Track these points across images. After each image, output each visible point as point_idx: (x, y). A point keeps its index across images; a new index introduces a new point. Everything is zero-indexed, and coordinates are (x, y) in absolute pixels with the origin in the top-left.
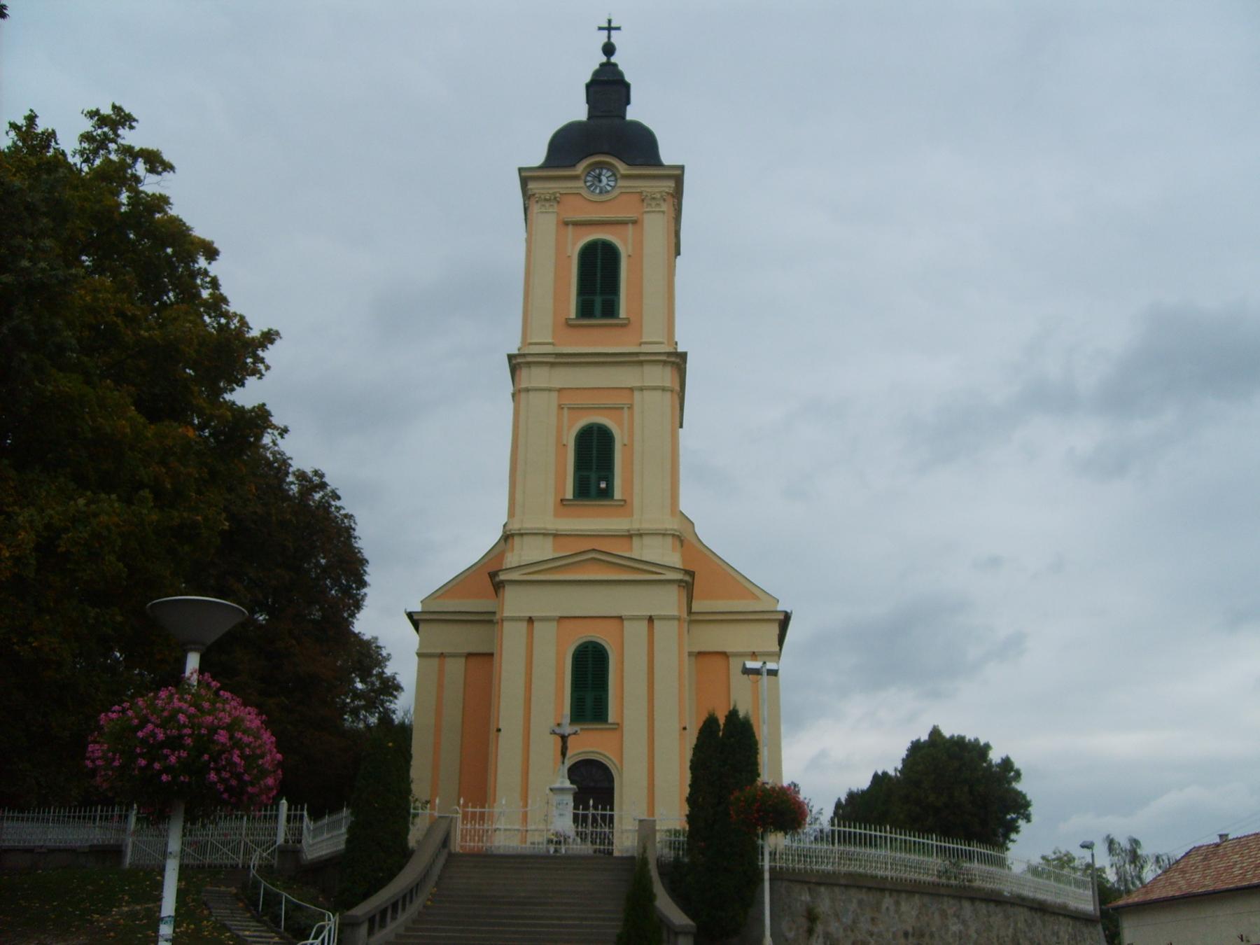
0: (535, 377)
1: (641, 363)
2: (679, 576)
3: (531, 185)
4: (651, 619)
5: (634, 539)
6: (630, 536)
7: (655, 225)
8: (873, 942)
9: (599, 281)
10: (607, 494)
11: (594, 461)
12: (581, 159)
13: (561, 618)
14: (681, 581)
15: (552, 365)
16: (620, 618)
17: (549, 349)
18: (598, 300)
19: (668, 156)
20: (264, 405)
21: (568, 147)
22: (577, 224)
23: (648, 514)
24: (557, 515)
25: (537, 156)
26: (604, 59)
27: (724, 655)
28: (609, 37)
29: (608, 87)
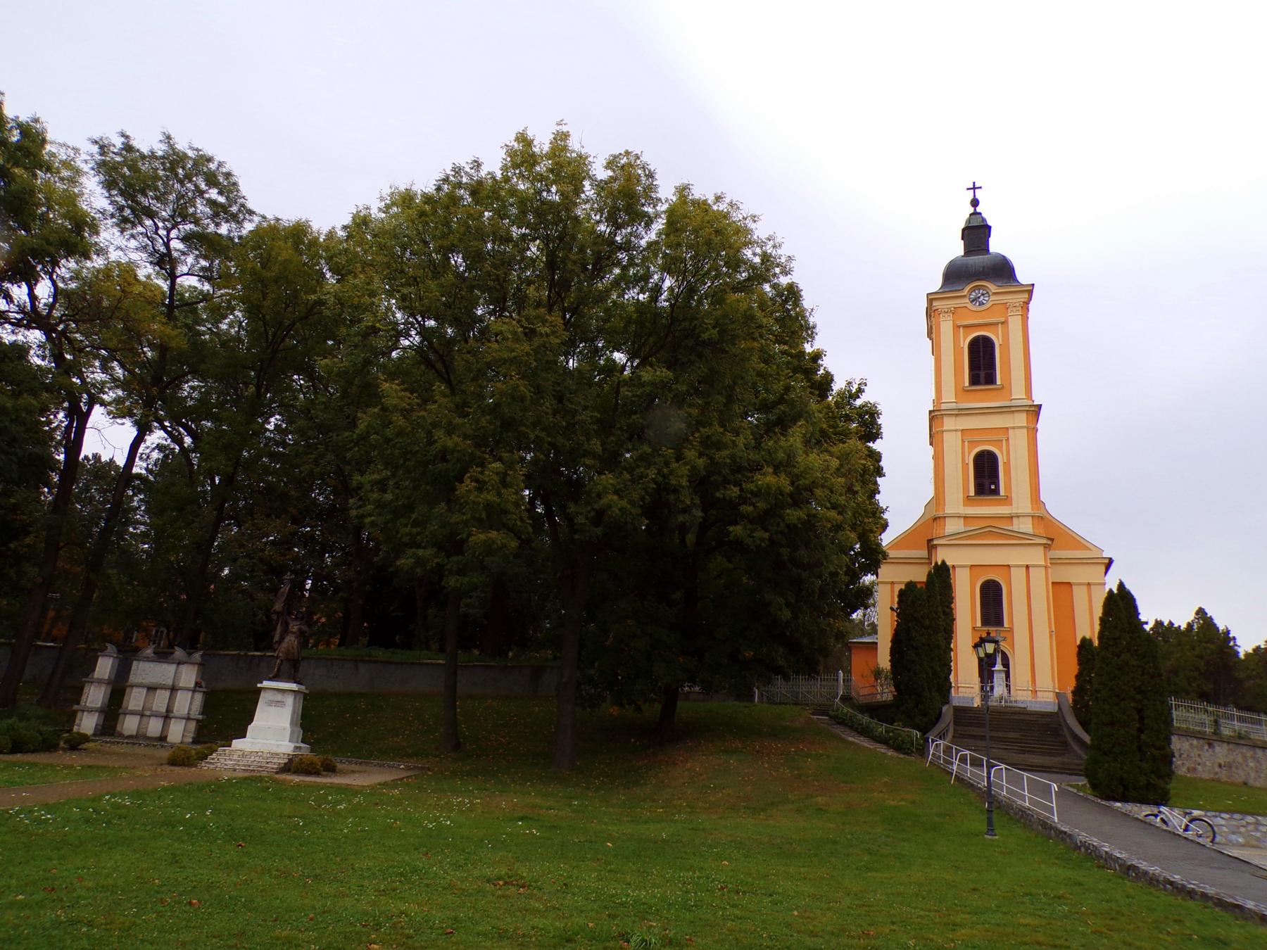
2: (1045, 541)
3: (935, 304)
4: (1027, 567)
5: (1015, 520)
7: (1015, 323)
9: (982, 362)
10: (996, 492)
11: (986, 473)
17: (953, 406)
18: (982, 374)
19: (1023, 276)
21: (955, 275)
22: (965, 327)
23: (1021, 503)
25: (936, 283)
26: (972, 210)
27: (1069, 584)
29: (976, 233)
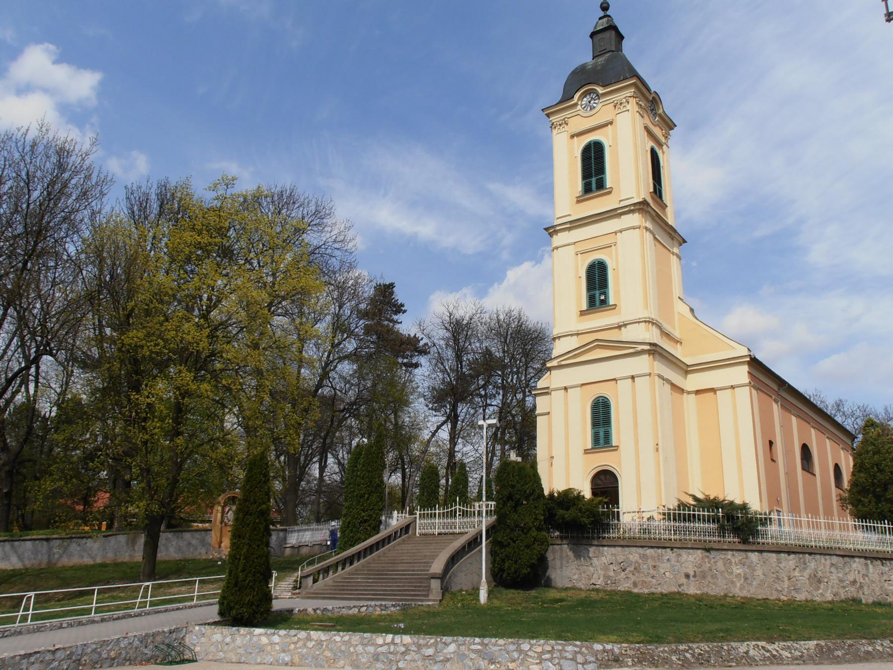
2: (647, 347)
8: (1, 259)
10: (604, 302)
15: (569, 229)
16: (614, 379)
20: (392, 285)
26: (602, 14)
27: (713, 390)
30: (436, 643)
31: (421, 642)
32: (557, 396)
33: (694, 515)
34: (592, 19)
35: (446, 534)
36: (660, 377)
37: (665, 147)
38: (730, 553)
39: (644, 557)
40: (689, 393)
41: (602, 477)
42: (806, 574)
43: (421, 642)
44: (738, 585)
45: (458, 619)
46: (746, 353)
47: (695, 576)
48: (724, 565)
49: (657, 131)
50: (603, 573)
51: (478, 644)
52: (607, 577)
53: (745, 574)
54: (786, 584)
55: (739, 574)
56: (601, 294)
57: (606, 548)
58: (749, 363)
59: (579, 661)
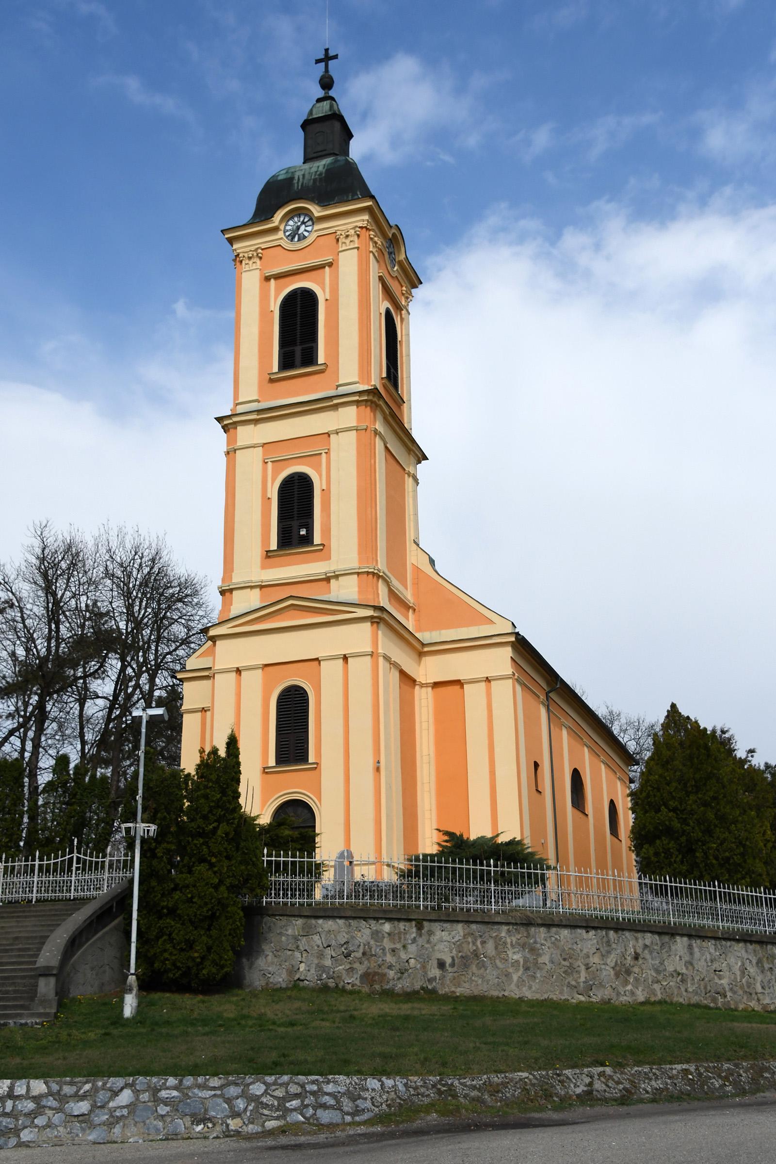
0: (246, 434)
1: (336, 407)
2: (370, 613)
5: (333, 581)
6: (328, 580)
10: (308, 540)
12: (277, 210)
13: (266, 665)
14: (372, 617)
15: (256, 422)
16: (317, 659)
17: (254, 406)
22: (278, 277)
24: (263, 567)
26: (321, 93)
27: (459, 683)
28: (327, 70)
30: (95, 1090)
31: (68, 1090)
32: (224, 683)
33: (475, 871)
34: (305, 98)
35: (55, 900)
36: (387, 658)
37: (404, 312)
38: (505, 928)
39: (376, 935)
40: (422, 685)
41: (290, 810)
42: (611, 960)
43: (68, 1090)
44: (515, 978)
45: (75, 1042)
46: (510, 630)
47: (453, 965)
48: (496, 948)
49: (394, 286)
50: (316, 961)
51: (175, 1088)
52: (321, 968)
53: (526, 961)
54: (583, 975)
55: (517, 961)
56: (301, 527)
57: (320, 921)
58: (512, 644)
59: (346, 1109)
